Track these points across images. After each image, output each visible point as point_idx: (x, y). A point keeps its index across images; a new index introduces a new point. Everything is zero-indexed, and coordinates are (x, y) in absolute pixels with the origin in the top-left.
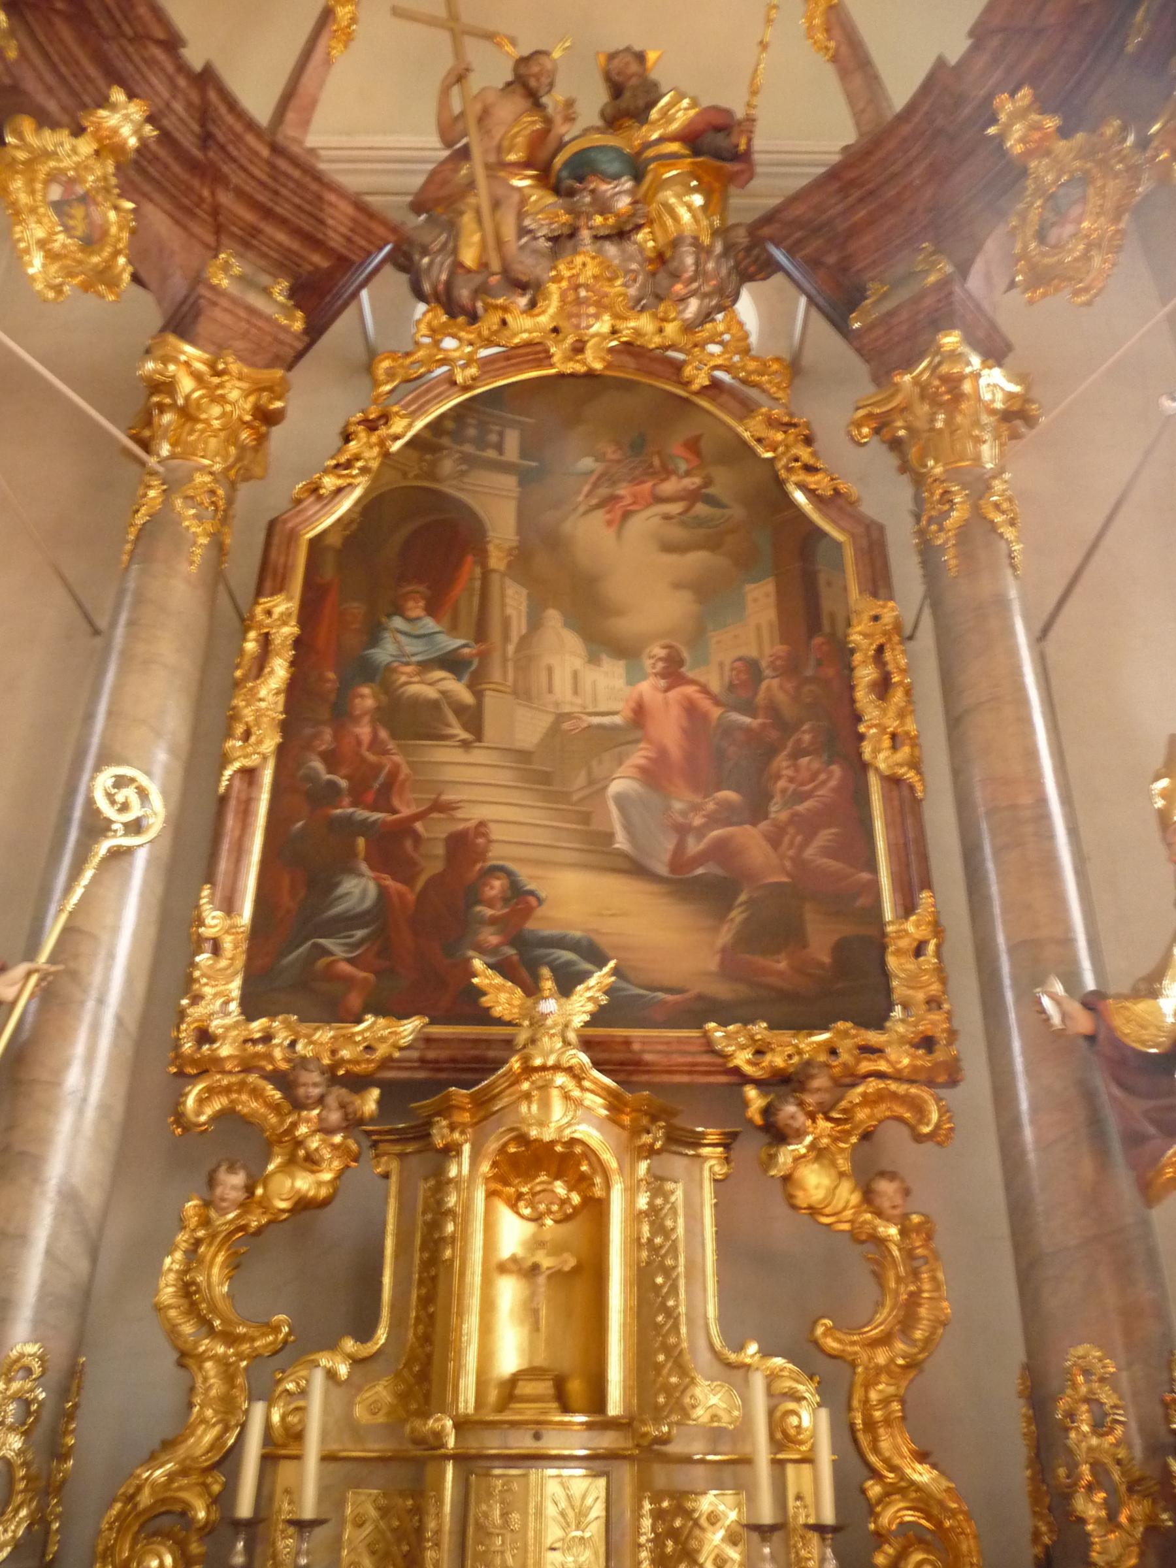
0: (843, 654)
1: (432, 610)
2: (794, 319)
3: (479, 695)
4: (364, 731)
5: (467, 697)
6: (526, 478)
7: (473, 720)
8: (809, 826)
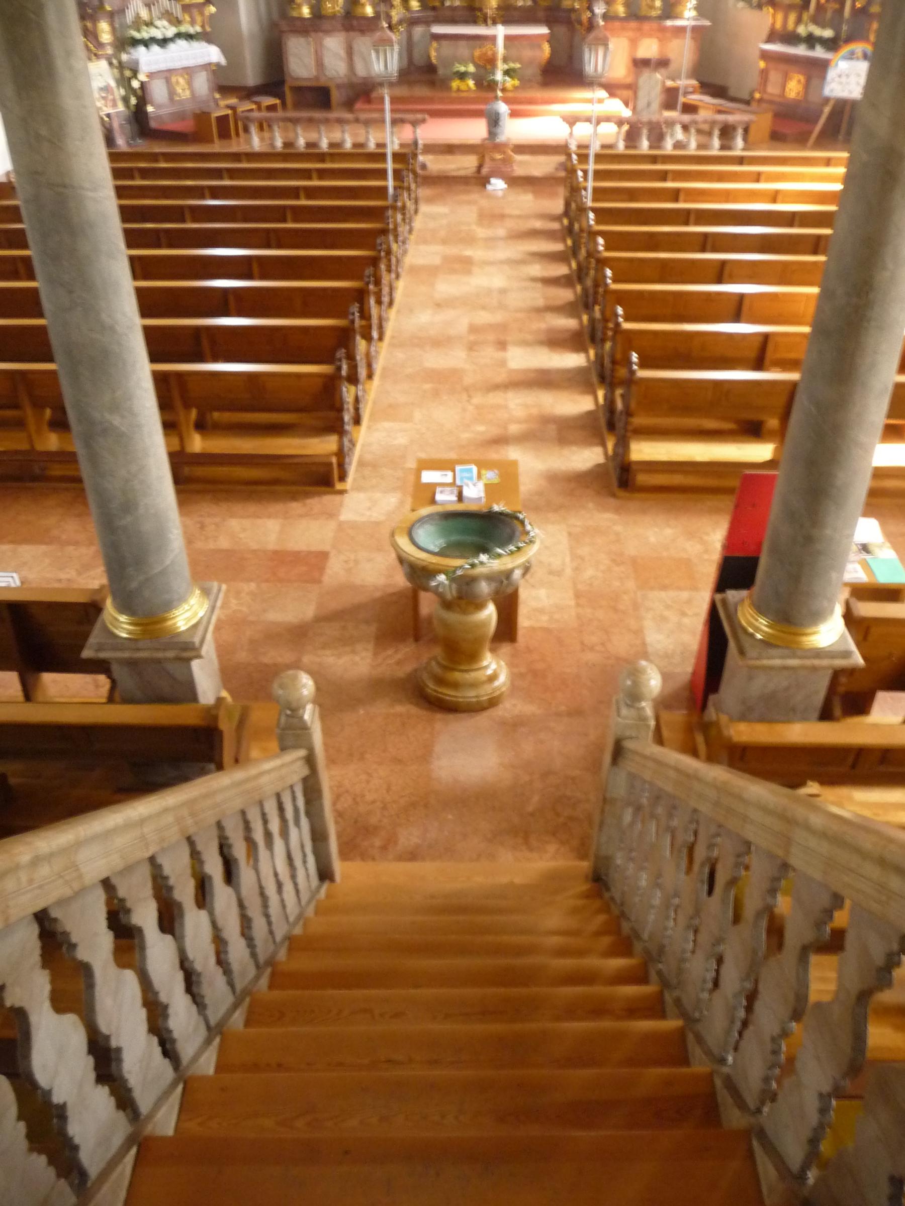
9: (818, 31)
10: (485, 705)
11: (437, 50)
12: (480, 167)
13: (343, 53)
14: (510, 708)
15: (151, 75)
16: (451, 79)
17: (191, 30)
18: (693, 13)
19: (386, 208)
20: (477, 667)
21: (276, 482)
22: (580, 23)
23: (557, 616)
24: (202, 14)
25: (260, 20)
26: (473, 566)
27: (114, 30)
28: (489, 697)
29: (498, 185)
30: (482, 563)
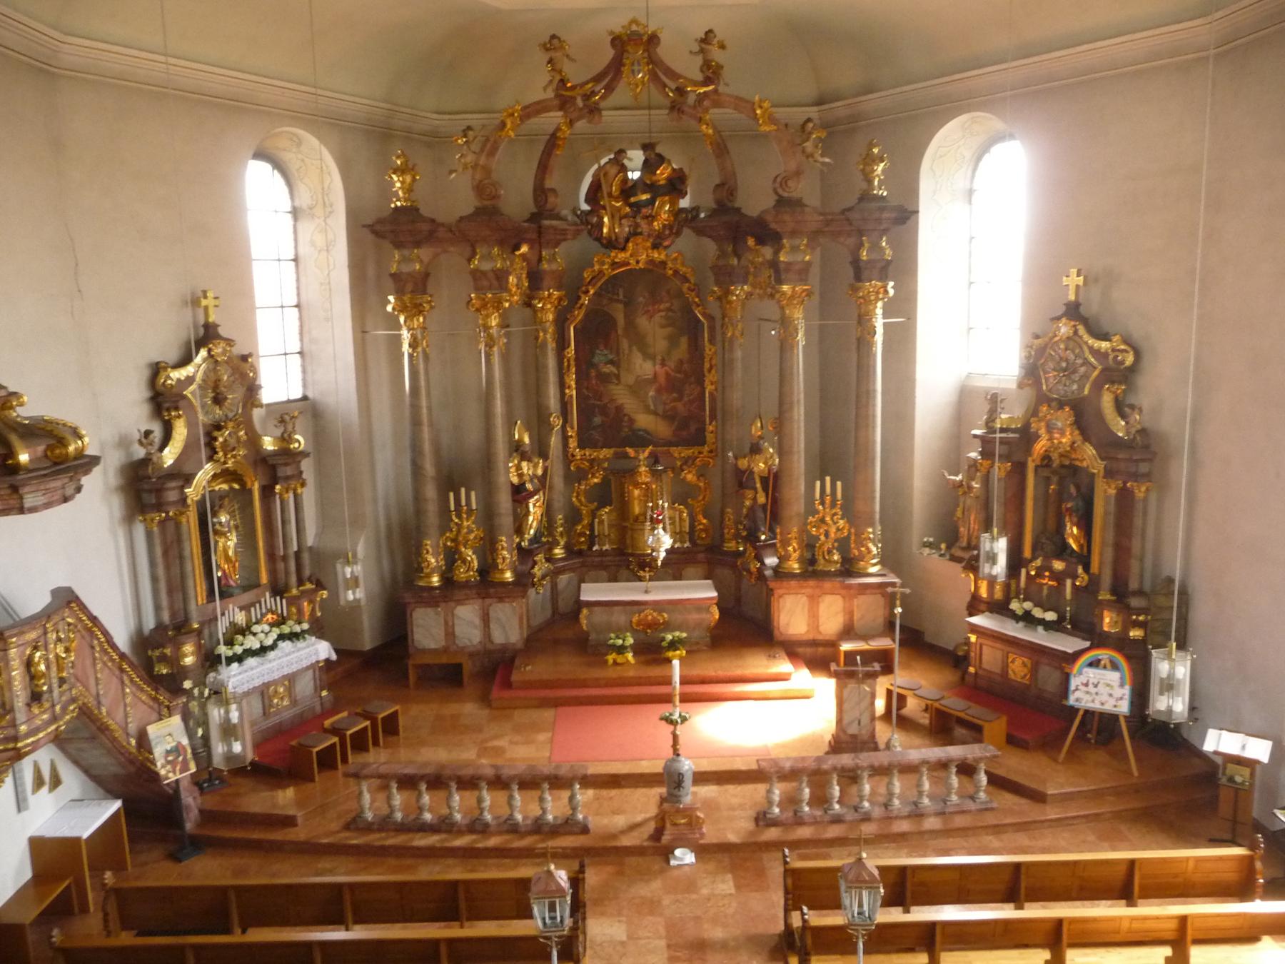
0: (702, 358)
1: (606, 347)
2: (286, 922)
3: (619, 371)
4: (594, 382)
5: (616, 372)
6: (626, 304)
7: (618, 377)
8: (691, 402)
9: (1038, 613)
13: (477, 621)
17: (297, 629)
25: (382, 579)
29: (683, 856)
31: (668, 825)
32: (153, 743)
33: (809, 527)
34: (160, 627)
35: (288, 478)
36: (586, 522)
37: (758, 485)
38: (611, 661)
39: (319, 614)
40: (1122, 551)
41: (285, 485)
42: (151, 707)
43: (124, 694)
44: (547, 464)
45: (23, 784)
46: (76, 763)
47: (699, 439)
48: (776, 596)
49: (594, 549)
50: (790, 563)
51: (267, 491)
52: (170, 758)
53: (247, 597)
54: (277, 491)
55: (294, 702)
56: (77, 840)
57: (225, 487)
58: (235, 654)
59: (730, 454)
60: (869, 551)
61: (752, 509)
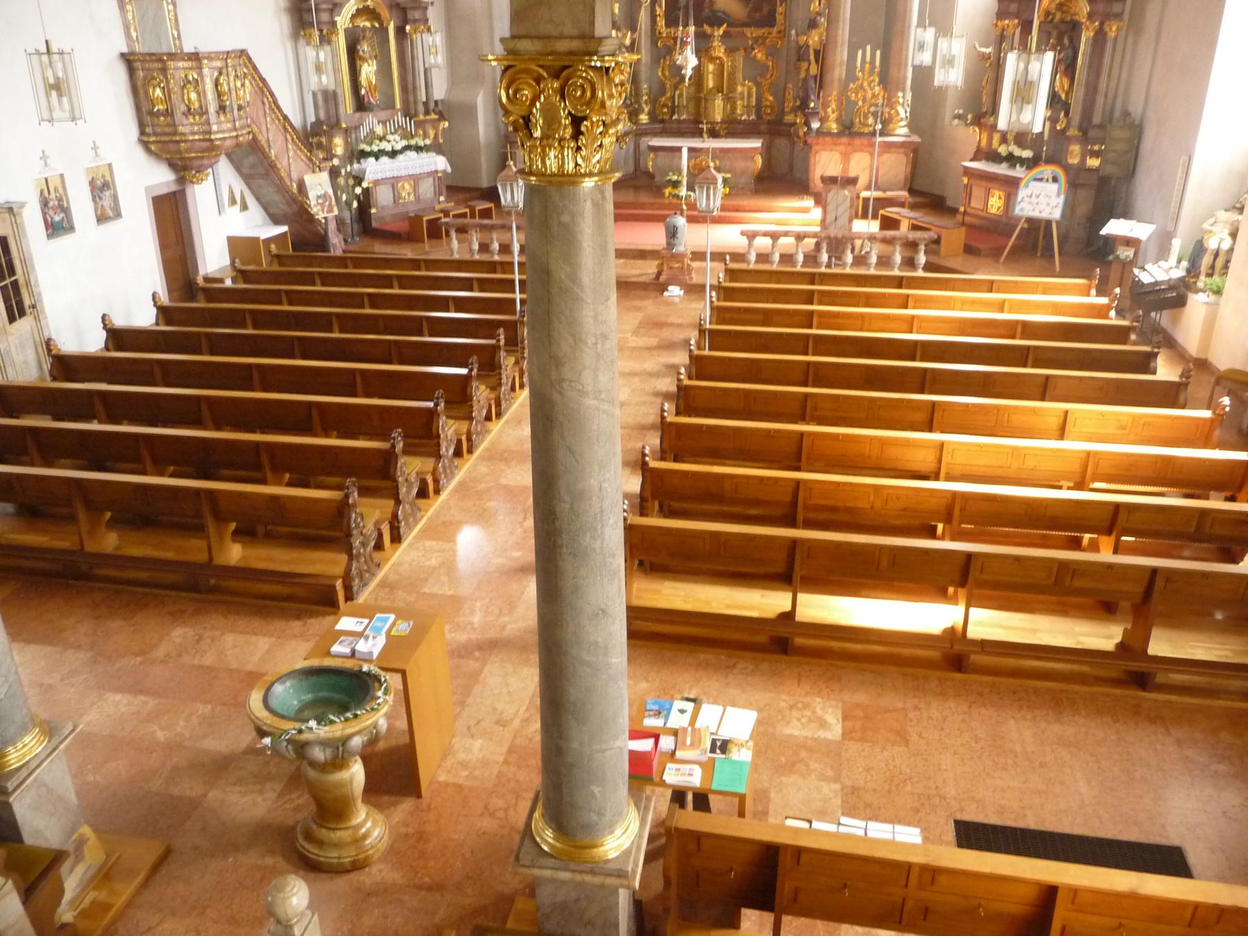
9: (1017, 152)
10: (350, 868)
11: (653, 160)
12: (659, 274)
14: (379, 873)
15: (377, 183)
16: (666, 187)
17: (421, 143)
18: (905, 131)
19: (515, 323)
20: (345, 826)
21: (289, 598)
22: (798, 137)
23: (477, 773)
24: (436, 128)
26: (300, 731)
27: (346, 143)
28: (352, 859)
29: (675, 291)
30: (311, 729)
31: (665, 268)
32: (308, 189)
33: (849, 93)
34: (318, 122)
35: (415, 21)
36: (668, 95)
37: (812, 57)
38: (667, 194)
39: (441, 141)
40: (1092, 90)
41: (414, 26)
42: (307, 165)
43: (288, 149)
44: (635, 36)
45: (222, 200)
46: (258, 199)
47: (769, 21)
48: (813, 152)
49: (674, 118)
50: (829, 123)
51: (400, 31)
52: (320, 201)
53: (384, 115)
54: (407, 31)
55: (418, 199)
56: (257, 239)
57: (368, 24)
58: (372, 151)
59: (793, 32)
60: (898, 114)
61: (805, 80)
